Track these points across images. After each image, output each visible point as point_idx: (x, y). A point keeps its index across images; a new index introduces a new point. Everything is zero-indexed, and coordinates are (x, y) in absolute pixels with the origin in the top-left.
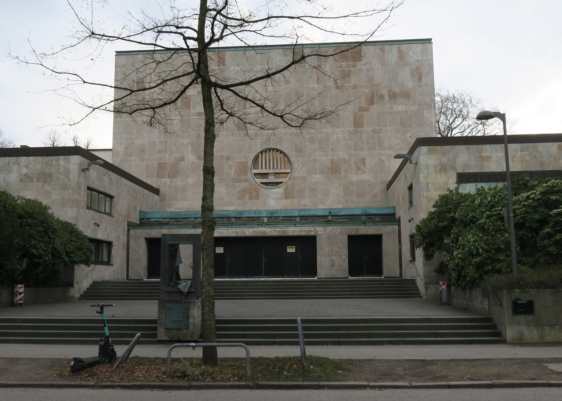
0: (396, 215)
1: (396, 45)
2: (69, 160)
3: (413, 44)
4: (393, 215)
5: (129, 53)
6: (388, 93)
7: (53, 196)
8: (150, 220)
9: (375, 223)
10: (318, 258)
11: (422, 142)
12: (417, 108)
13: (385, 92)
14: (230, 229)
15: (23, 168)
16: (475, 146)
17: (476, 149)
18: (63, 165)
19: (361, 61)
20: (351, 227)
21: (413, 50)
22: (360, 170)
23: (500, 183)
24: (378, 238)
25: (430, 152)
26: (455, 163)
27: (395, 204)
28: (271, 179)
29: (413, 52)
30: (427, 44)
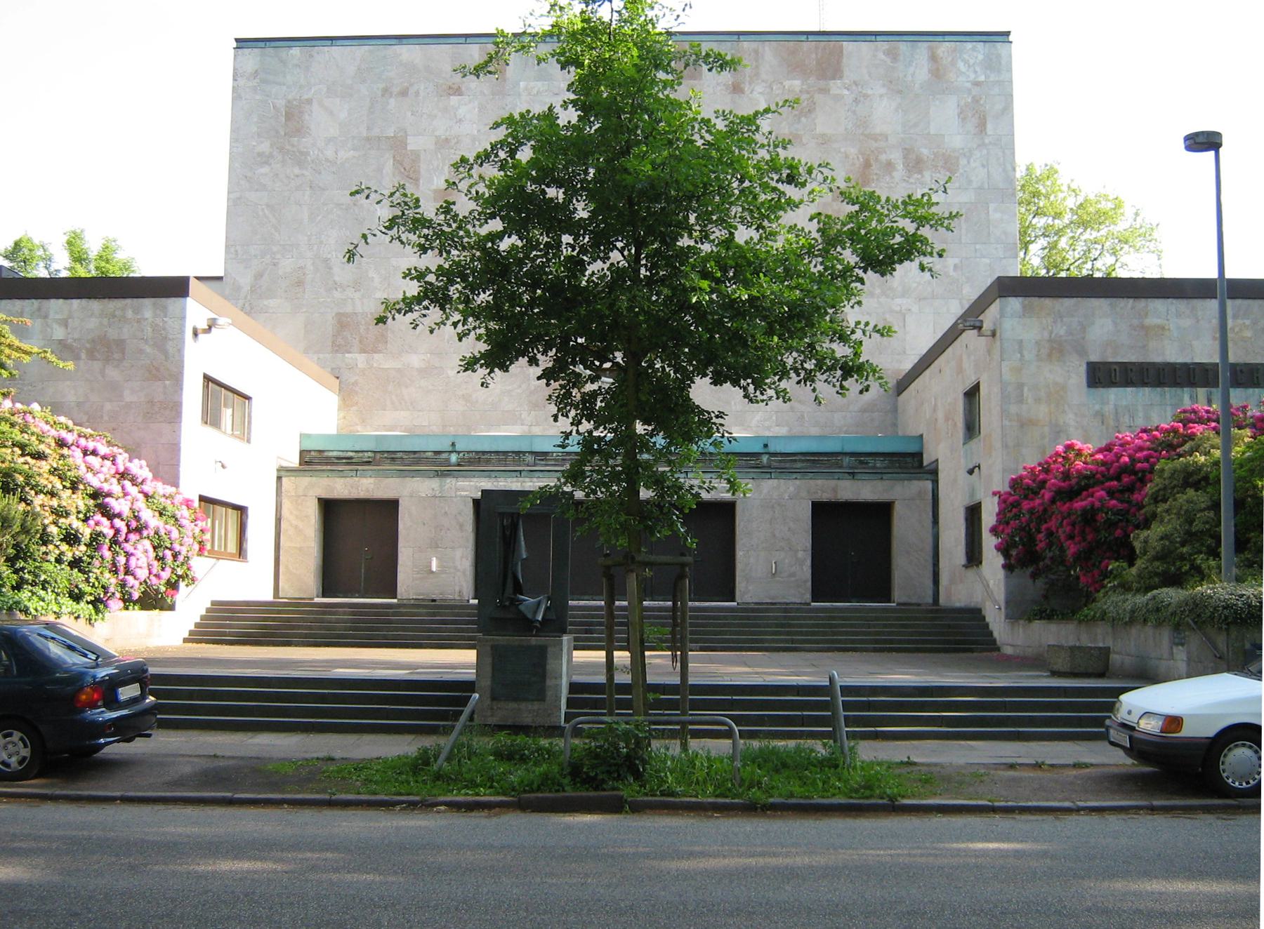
0: (924, 456)
1: (926, 45)
2: (164, 309)
3: (965, 44)
4: (919, 455)
5: (268, 43)
6: (905, 157)
7: (127, 393)
8: (326, 454)
9: (879, 474)
10: (740, 554)
11: (1009, 287)
12: (973, 197)
13: (896, 156)
14: (527, 479)
15: (55, 326)
16: (1131, 301)
17: (1133, 308)
18: (150, 320)
19: (841, 78)
20: (819, 482)
21: (966, 56)
23: (1185, 389)
24: (882, 512)
25: (1027, 311)
26: (1083, 338)
27: (921, 429)
29: (966, 62)
30: (998, 45)
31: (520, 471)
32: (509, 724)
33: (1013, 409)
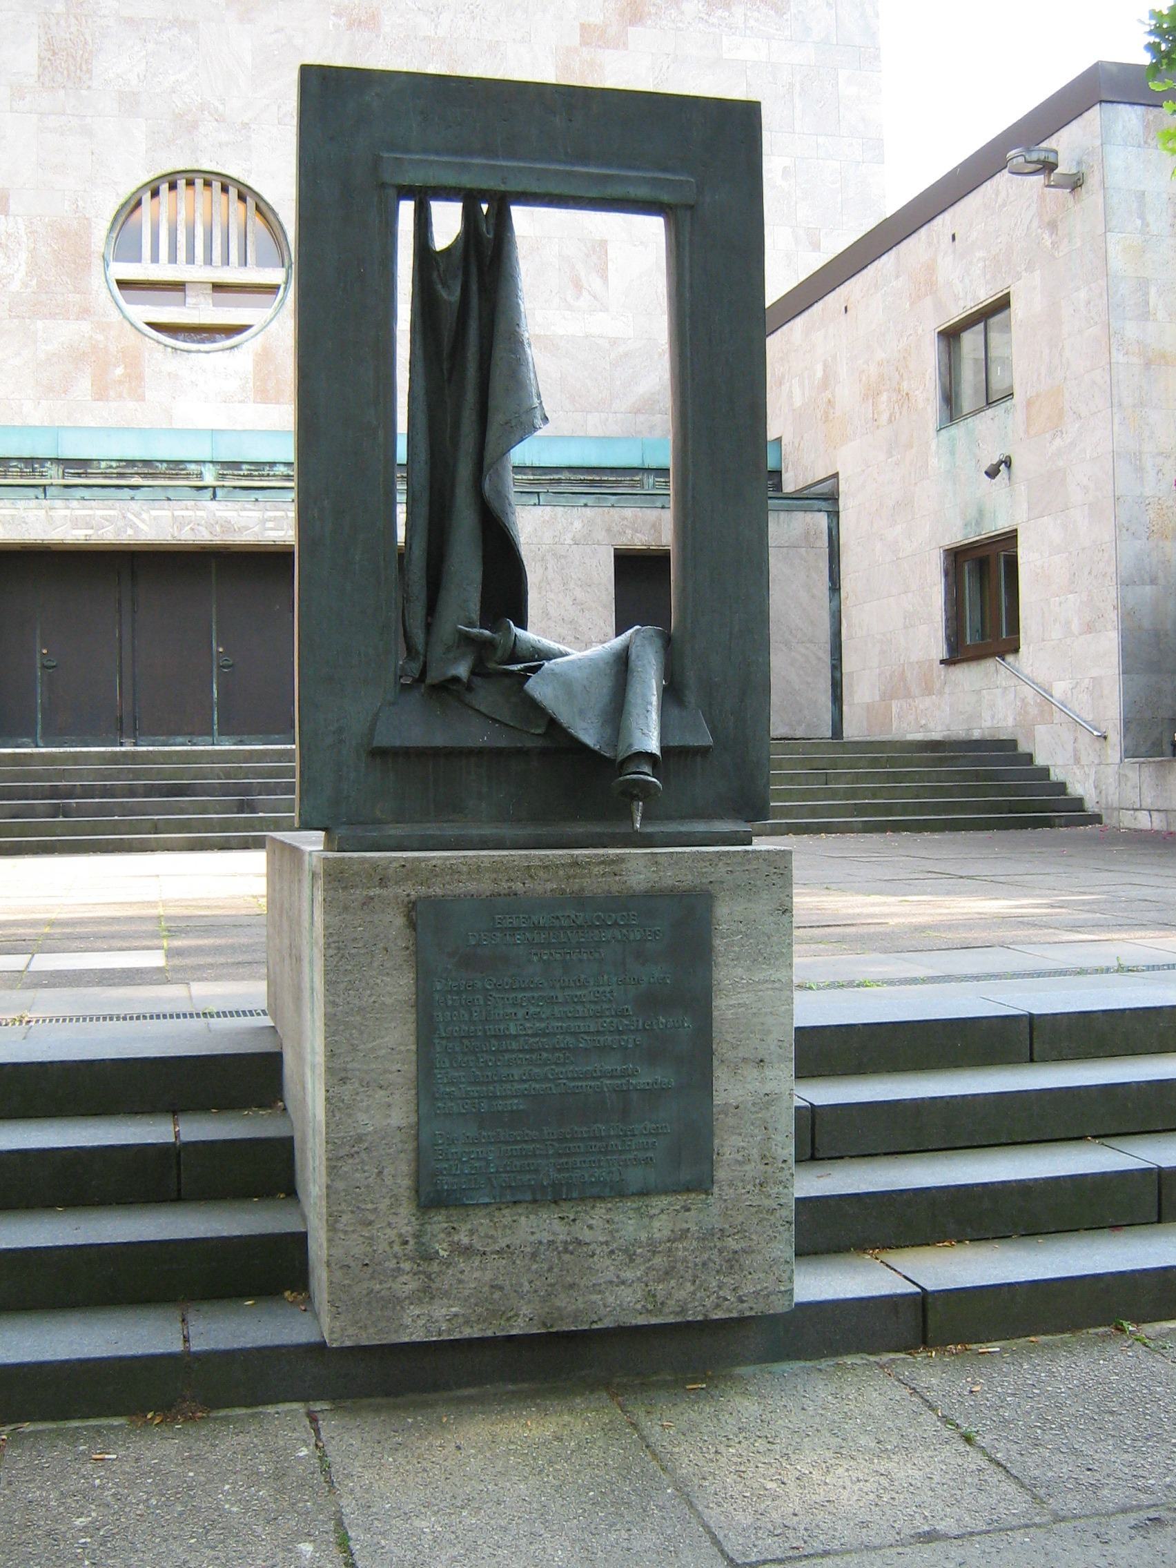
14: (58, 503)
20: (628, 513)
22: (585, 293)
28: (201, 311)
31: (44, 486)
32: (518, 1328)
33: (1131, 330)
